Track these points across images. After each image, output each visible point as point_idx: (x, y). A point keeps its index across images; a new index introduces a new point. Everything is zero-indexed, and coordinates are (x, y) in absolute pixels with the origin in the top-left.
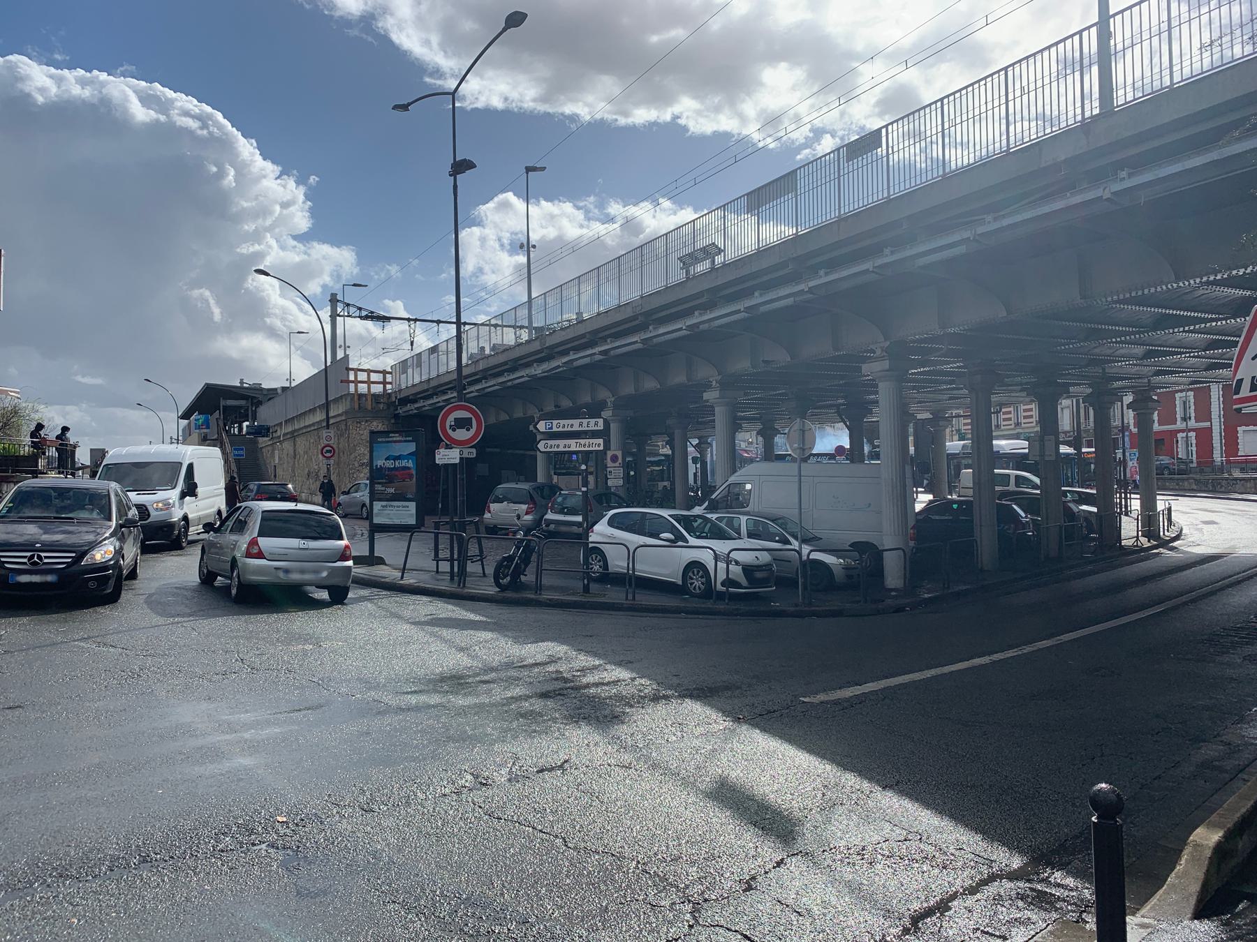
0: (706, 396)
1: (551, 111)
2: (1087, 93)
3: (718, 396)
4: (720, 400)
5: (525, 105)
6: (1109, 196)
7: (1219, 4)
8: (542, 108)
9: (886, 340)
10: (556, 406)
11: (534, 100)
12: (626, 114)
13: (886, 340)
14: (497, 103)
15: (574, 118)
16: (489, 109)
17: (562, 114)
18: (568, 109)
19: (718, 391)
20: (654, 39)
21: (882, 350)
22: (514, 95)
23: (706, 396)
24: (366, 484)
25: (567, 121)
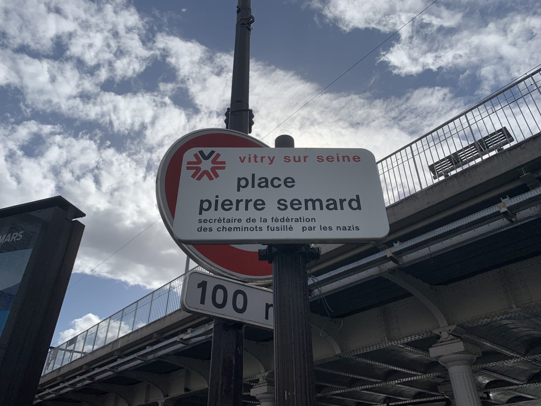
0: (253, 392)
1: (115, 278)
2: (469, 133)
3: (266, 391)
4: (267, 395)
5: (102, 274)
6: (391, 255)
7: (458, 134)
8: (110, 276)
9: (266, 371)
10: (186, 390)
11: (108, 272)
12: (150, 284)
13: (266, 371)
14: (87, 271)
15: (125, 283)
16: (83, 274)
17: (120, 280)
18: (123, 278)
19: (266, 386)
20: (163, 252)
21: (263, 379)
22: (97, 269)
23: (253, 392)
24: (385, 247)
25: (124, 285)
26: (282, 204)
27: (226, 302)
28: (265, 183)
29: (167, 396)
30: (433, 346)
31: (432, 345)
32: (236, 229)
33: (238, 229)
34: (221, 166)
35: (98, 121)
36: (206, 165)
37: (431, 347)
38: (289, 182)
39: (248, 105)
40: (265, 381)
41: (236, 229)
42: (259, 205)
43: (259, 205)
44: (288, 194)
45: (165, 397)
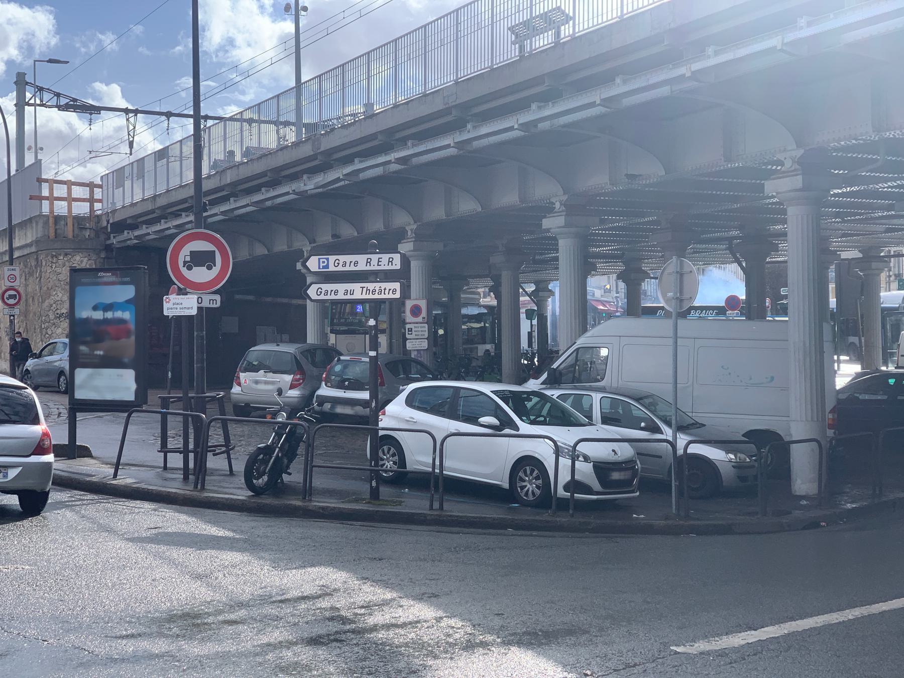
26: (180, 309)
27: (516, 461)
28: (178, 304)
29: (314, 242)
30: (402, 241)
31: (401, 241)
32: (212, 301)
33: (215, 301)
34: (170, 300)
35: (50, 124)
36: (167, 300)
37: (400, 243)
38: (181, 304)
39: (100, 320)
40: (798, 167)
41: (212, 301)
42: (177, 309)
43: (177, 309)
44: (181, 306)
45: (310, 244)
